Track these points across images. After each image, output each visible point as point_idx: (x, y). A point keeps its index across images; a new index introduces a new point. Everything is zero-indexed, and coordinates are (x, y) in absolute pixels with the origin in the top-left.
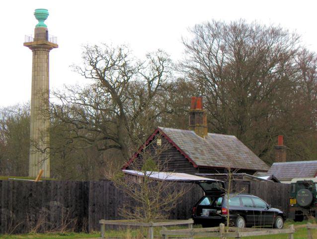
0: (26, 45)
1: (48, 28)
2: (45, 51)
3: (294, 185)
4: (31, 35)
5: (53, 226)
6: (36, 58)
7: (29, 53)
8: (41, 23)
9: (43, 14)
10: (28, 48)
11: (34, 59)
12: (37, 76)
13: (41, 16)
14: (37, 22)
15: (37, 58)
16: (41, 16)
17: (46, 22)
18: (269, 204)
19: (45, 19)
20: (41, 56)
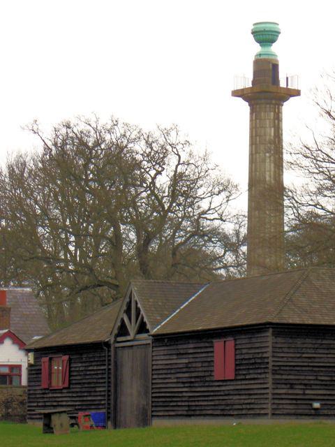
0: (237, 93)
1: (279, 58)
2: (270, 104)
3: (281, 207)
4: (246, 79)
5: (14, 405)
6: (254, 118)
7: (243, 107)
8: (266, 50)
9: (265, 31)
10: (240, 100)
11: (251, 113)
12: (256, 153)
13: (265, 36)
14: (257, 48)
15: (256, 119)
16: (265, 36)
17: (275, 48)
18: (191, 252)
19: (273, 41)
20: (263, 114)
